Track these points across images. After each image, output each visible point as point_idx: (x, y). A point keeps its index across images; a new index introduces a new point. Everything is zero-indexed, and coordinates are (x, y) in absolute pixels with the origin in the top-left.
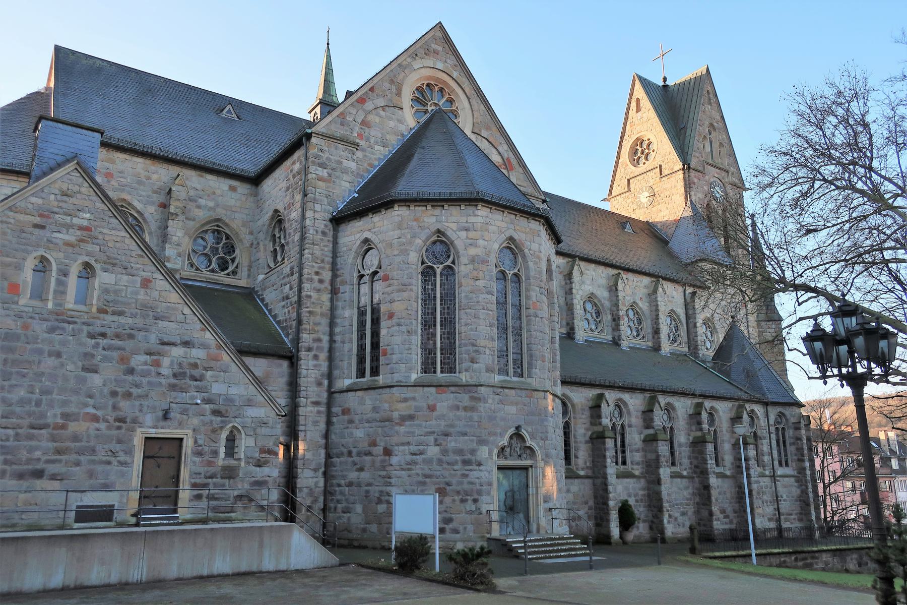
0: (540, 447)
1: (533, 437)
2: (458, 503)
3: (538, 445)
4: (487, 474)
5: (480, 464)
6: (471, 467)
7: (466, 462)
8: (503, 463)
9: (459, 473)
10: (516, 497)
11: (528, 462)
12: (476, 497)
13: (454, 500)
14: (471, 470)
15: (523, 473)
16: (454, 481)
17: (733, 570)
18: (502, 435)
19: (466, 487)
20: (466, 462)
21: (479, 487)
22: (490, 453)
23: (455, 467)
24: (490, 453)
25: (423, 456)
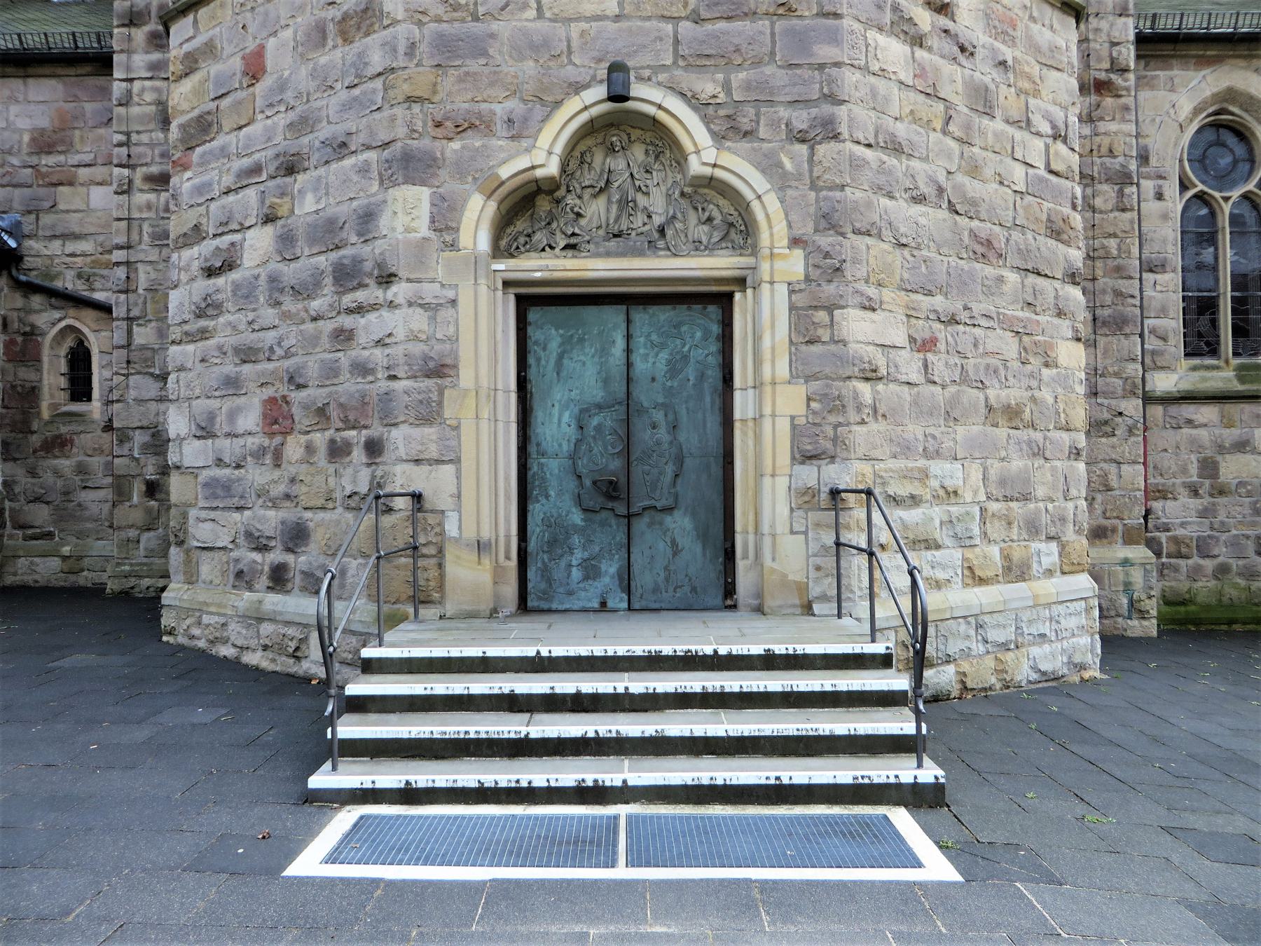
0: (782, 181)
1: (730, 128)
2: (321, 457)
3: (770, 167)
4: (418, 320)
5: (387, 279)
6: (361, 296)
7: (347, 276)
8: (542, 266)
9: (327, 326)
10: (643, 436)
11: (717, 264)
12: (376, 430)
13: (310, 449)
14: (359, 310)
15: (705, 322)
16: (312, 368)
17: (772, 309)
18: (520, 130)
19: (349, 386)
20: (347, 276)
21: (384, 385)
22: (444, 221)
23: (316, 305)
24: (444, 221)
25: (234, 276)
